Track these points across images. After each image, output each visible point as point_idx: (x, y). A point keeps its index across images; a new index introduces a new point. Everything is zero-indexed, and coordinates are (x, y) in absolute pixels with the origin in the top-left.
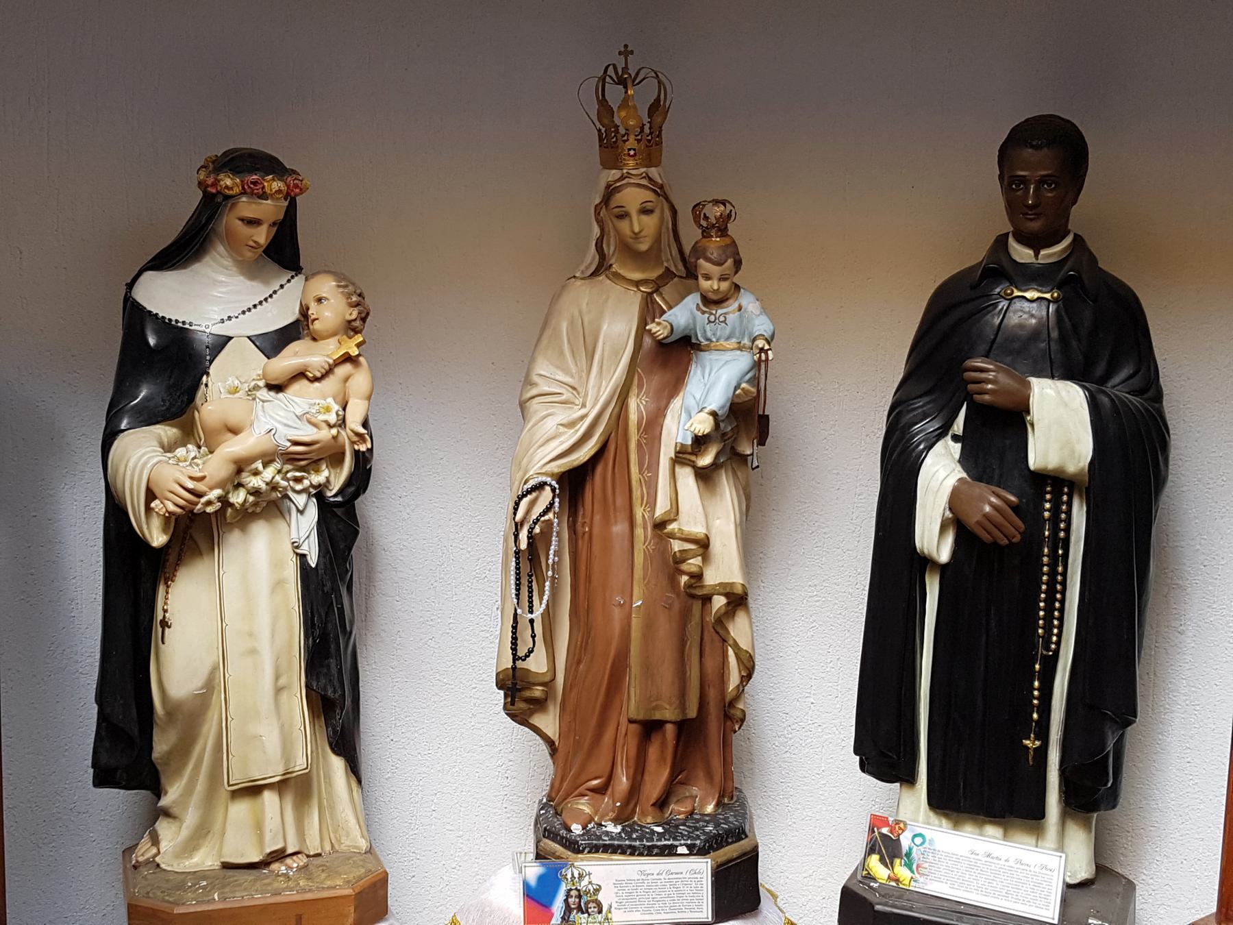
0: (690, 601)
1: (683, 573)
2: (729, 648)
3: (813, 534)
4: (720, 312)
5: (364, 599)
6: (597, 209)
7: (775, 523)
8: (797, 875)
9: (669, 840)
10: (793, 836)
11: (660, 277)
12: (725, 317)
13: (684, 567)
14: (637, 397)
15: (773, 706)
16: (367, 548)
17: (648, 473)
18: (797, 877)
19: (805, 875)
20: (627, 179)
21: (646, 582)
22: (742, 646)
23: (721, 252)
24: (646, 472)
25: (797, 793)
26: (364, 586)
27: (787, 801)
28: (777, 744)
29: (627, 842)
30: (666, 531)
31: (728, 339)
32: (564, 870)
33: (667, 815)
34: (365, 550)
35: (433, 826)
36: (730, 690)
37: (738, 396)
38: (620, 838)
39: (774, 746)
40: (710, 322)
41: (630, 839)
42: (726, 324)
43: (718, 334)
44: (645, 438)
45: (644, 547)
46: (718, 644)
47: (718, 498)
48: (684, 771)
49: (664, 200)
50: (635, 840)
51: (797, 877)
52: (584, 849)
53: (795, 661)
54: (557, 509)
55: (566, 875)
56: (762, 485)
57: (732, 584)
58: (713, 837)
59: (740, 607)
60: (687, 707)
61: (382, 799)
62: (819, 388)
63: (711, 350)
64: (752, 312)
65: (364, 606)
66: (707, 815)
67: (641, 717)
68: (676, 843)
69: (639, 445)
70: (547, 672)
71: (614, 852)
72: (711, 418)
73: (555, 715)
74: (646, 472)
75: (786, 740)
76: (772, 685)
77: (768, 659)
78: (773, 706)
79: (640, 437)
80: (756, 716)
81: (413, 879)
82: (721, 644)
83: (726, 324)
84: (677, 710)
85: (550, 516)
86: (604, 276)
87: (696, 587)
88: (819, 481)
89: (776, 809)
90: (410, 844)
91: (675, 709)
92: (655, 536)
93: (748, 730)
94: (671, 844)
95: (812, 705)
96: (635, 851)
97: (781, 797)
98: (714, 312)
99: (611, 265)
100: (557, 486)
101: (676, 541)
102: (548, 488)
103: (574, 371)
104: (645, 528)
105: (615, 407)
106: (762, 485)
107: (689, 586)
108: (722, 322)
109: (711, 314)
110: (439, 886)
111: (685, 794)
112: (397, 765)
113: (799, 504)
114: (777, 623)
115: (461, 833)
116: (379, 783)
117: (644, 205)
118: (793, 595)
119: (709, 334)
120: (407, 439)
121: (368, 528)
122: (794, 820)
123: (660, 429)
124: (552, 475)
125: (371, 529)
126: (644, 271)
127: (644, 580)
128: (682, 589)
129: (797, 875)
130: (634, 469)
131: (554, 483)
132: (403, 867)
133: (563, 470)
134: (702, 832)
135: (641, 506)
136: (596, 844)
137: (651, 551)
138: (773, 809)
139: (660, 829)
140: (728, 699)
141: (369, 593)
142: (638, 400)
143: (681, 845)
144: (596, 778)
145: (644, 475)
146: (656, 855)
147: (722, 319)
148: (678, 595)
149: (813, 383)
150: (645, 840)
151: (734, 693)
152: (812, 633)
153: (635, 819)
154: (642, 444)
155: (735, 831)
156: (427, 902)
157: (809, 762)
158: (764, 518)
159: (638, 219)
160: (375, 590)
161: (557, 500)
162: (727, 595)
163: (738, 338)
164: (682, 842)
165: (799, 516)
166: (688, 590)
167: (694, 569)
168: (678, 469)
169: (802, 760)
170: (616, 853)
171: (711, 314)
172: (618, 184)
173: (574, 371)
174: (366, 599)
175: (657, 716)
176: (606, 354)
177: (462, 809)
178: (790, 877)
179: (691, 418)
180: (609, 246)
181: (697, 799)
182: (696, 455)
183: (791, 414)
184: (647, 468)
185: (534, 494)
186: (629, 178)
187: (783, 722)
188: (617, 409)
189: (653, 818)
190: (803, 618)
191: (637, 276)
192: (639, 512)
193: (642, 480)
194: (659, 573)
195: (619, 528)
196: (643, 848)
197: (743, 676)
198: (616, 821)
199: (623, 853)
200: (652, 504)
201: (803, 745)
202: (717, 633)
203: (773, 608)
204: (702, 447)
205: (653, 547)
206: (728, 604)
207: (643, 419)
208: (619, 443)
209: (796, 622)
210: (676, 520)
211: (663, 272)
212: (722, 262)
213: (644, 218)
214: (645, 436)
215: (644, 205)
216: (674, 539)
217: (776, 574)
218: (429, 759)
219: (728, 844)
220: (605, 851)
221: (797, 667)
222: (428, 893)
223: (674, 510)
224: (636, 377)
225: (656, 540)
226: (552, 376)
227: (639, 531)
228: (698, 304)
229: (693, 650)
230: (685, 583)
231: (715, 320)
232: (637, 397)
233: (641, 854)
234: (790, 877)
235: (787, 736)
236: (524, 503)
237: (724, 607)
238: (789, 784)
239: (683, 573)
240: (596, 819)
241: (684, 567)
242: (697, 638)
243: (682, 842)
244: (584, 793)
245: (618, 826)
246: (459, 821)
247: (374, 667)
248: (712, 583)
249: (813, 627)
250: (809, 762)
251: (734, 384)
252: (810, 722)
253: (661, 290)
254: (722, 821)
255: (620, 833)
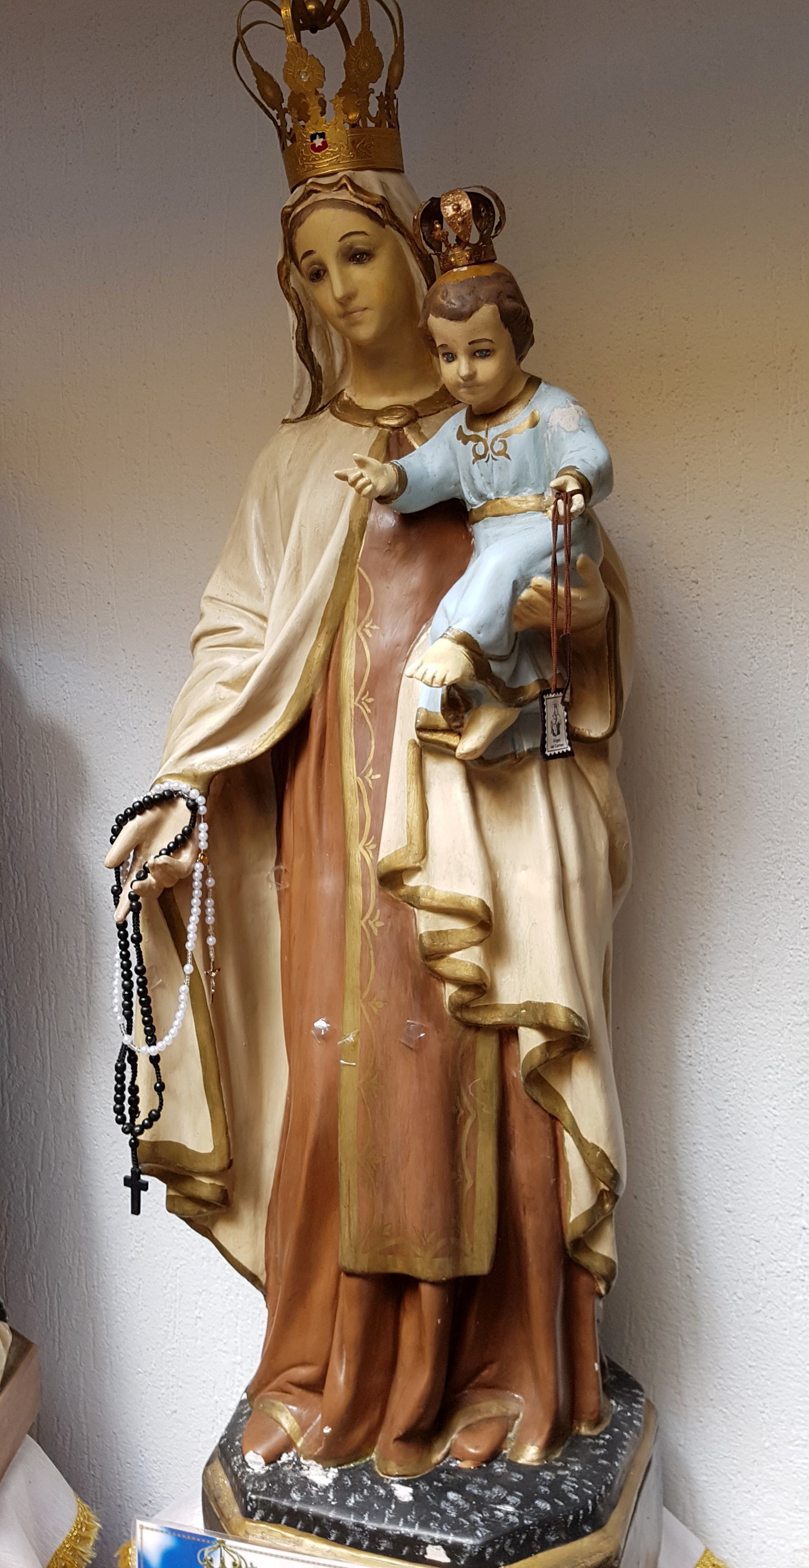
0: (469, 1036)
1: (443, 979)
2: (566, 1134)
3: (799, 903)
4: (494, 431)
5: (85, 983)
6: (284, 278)
7: (725, 879)
8: (782, 1542)
9: (412, 1526)
10: (772, 1469)
11: (424, 403)
12: (505, 443)
13: (443, 967)
14: (358, 624)
15: (732, 1223)
16: (86, 906)
17: (374, 774)
18: (782, 1545)
19: (796, 1545)
20: (314, 195)
21: (366, 994)
22: (585, 1136)
23: (464, 291)
24: (371, 771)
25: (780, 1391)
26: (84, 964)
27: (761, 1403)
28: (740, 1295)
29: (332, 1514)
30: (403, 891)
31: (516, 488)
32: (207, 1551)
33: (438, 1457)
34: (83, 907)
35: (199, 1342)
36: (571, 1219)
37: (529, 604)
38: (323, 1500)
39: (735, 1298)
40: (479, 457)
41: (341, 1506)
42: (508, 457)
43: (496, 480)
44: (368, 704)
45: (363, 923)
46: (541, 1126)
47: (524, 824)
48: (491, 1362)
49: (396, 233)
50: (349, 1510)
51: (782, 1545)
52: (254, 1510)
53: (771, 1145)
54: (203, 845)
55: (211, 1560)
56: (699, 809)
57: (547, 1007)
58: (507, 1535)
59: (579, 1053)
60: (468, 1251)
61: (125, 1290)
62: (800, 619)
63: (487, 516)
64: (559, 426)
65: (85, 993)
66: (520, 1468)
67: (363, 1266)
68: (425, 1534)
69: (359, 718)
70: (213, 1152)
71: (307, 1529)
72: (461, 649)
73: (256, 1228)
74: (371, 771)
75: (757, 1290)
76: (728, 1184)
77: (722, 1137)
78: (732, 1223)
79: (360, 702)
80: (702, 1238)
81: (175, 1415)
82: (548, 1125)
83: (508, 457)
84: (438, 1261)
85: (186, 857)
86: (328, 410)
87: (477, 1009)
88: (805, 800)
89: (741, 1412)
90: (169, 1362)
91: (435, 1256)
92: (383, 900)
93: (688, 1261)
94: (416, 1537)
95: (804, 1233)
96: (347, 1535)
97: (750, 1392)
98: (482, 434)
99: (342, 392)
100: (201, 800)
101: (422, 912)
102: (182, 803)
103: (262, 586)
104: (365, 886)
105: (315, 645)
106: (699, 809)
107: (460, 1007)
108: (498, 454)
109: (478, 439)
110: (212, 1433)
111: (488, 1411)
112: (144, 1242)
113: (770, 844)
114: (736, 1069)
115: (239, 1358)
116: (120, 1265)
117: (348, 240)
118: (762, 1018)
119: (479, 483)
120: (137, 737)
121: (86, 874)
122: (774, 1441)
123: (397, 684)
124: (195, 778)
125: (90, 876)
126: (394, 393)
127: (362, 989)
128: (447, 1010)
129: (782, 1542)
130: (350, 765)
131: (195, 794)
132: (160, 1396)
133: (215, 768)
134: (487, 1515)
135: (360, 840)
136: (275, 1505)
137: (376, 932)
138: (736, 1412)
139: (404, 1493)
140: (569, 1236)
141: (91, 975)
142: (360, 628)
143: (434, 1543)
144: (304, 1364)
145: (367, 777)
146: (386, 1553)
147: (498, 447)
148: (439, 1023)
149: (788, 610)
150: (366, 1516)
151: (581, 1227)
152: (800, 1095)
153: (374, 1456)
154: (363, 717)
155: (566, 1517)
156: (196, 1453)
157: (800, 1338)
158: (705, 870)
159: (341, 273)
160: (100, 971)
161: (203, 827)
162: (544, 1028)
163: (535, 486)
164: (437, 1536)
165: (770, 867)
166: (458, 1015)
167: (466, 973)
168: (432, 765)
169: (787, 1332)
170: (311, 1532)
171: (478, 439)
172: (299, 209)
173: (262, 586)
174: (88, 983)
175: (399, 1267)
176: (306, 545)
177: (240, 1322)
178: (769, 1543)
179: (265, 619)
180: (329, 353)
181: (517, 1422)
182: (460, 735)
183: (747, 672)
184: (373, 764)
185: (150, 815)
186: (317, 192)
187: (751, 1256)
188: (321, 650)
189: (399, 1464)
190: (783, 1065)
191: (382, 402)
192: (358, 851)
193: (363, 787)
194: (393, 978)
195: (328, 884)
196: (361, 1533)
197: (603, 1191)
198: (326, 1459)
199: (324, 1535)
200: (376, 835)
201: (789, 1304)
202: (536, 1102)
203: (727, 1040)
204: (466, 716)
205: (380, 924)
206: (548, 1046)
207: (366, 665)
208: (328, 716)
209: (770, 1070)
210: (419, 869)
211: (436, 393)
212: (466, 309)
213: (358, 273)
214: (370, 700)
215: (348, 240)
216: (419, 908)
217: (731, 977)
218: (187, 1237)
219: (546, 1546)
220: (291, 1524)
221: (774, 1156)
222: (195, 1440)
223: (416, 848)
224: (356, 586)
225: (387, 909)
226: (229, 599)
227: (356, 891)
228: (460, 427)
229: (480, 1134)
230: (450, 998)
231: (486, 450)
232: (358, 624)
233: (356, 1546)
234: (769, 1543)
235: (758, 1282)
236: (130, 828)
237: (538, 1053)
238: (764, 1373)
239: (443, 979)
240: (299, 1444)
241: (443, 967)
242: (488, 1111)
243: (437, 1536)
244: (285, 1389)
245: (332, 1469)
246: (236, 1339)
247: (104, 1088)
248: (514, 1002)
249: (802, 1083)
250: (800, 1338)
251: (511, 575)
252: (800, 1263)
253: (419, 421)
254: (543, 1489)
255: (326, 1490)
